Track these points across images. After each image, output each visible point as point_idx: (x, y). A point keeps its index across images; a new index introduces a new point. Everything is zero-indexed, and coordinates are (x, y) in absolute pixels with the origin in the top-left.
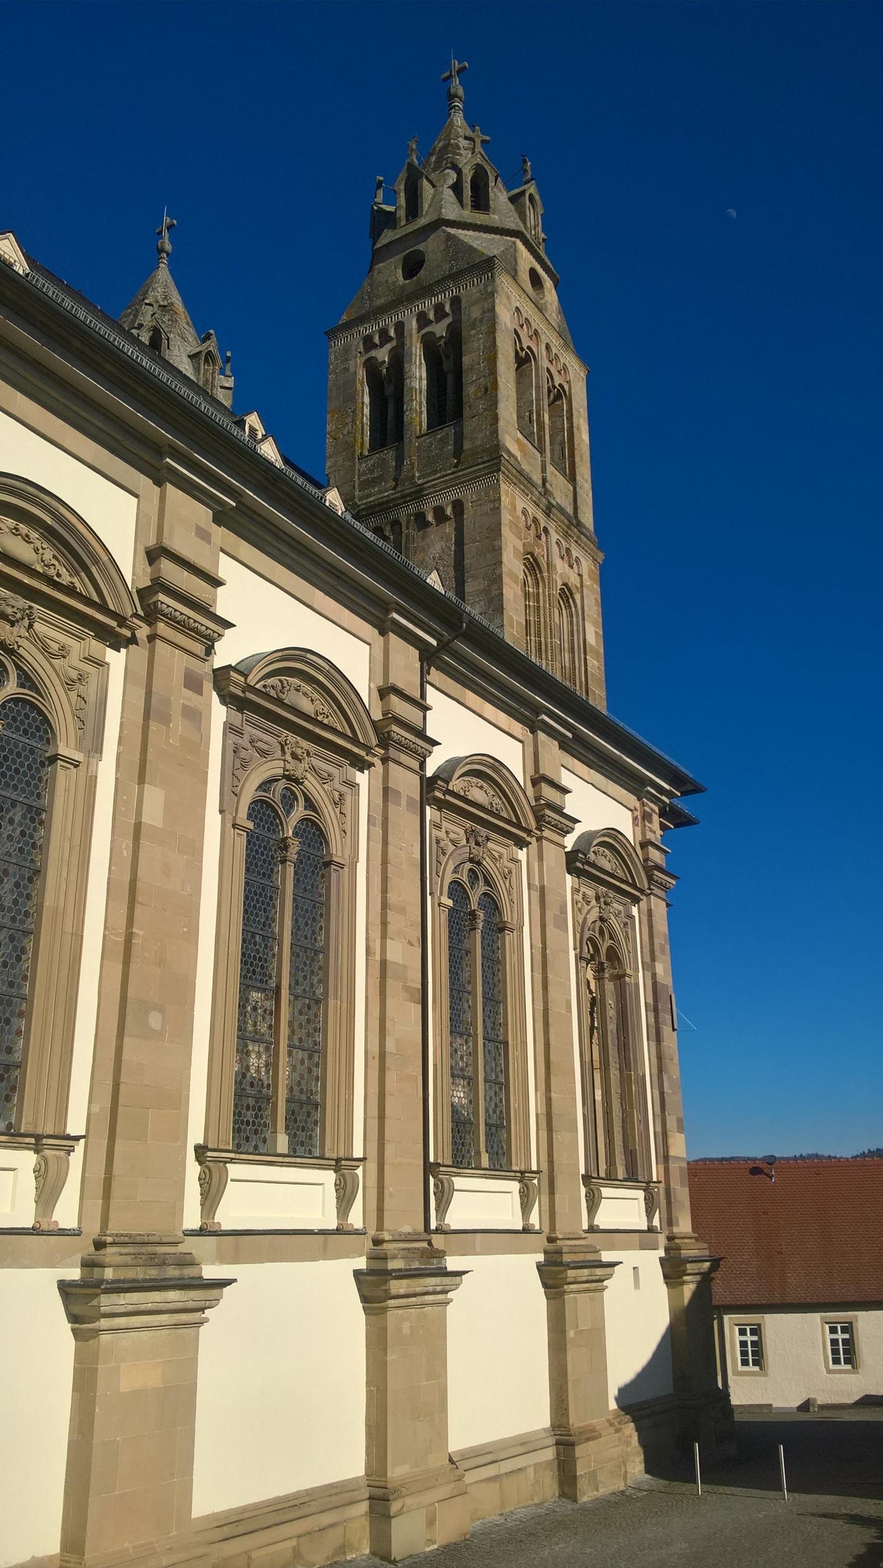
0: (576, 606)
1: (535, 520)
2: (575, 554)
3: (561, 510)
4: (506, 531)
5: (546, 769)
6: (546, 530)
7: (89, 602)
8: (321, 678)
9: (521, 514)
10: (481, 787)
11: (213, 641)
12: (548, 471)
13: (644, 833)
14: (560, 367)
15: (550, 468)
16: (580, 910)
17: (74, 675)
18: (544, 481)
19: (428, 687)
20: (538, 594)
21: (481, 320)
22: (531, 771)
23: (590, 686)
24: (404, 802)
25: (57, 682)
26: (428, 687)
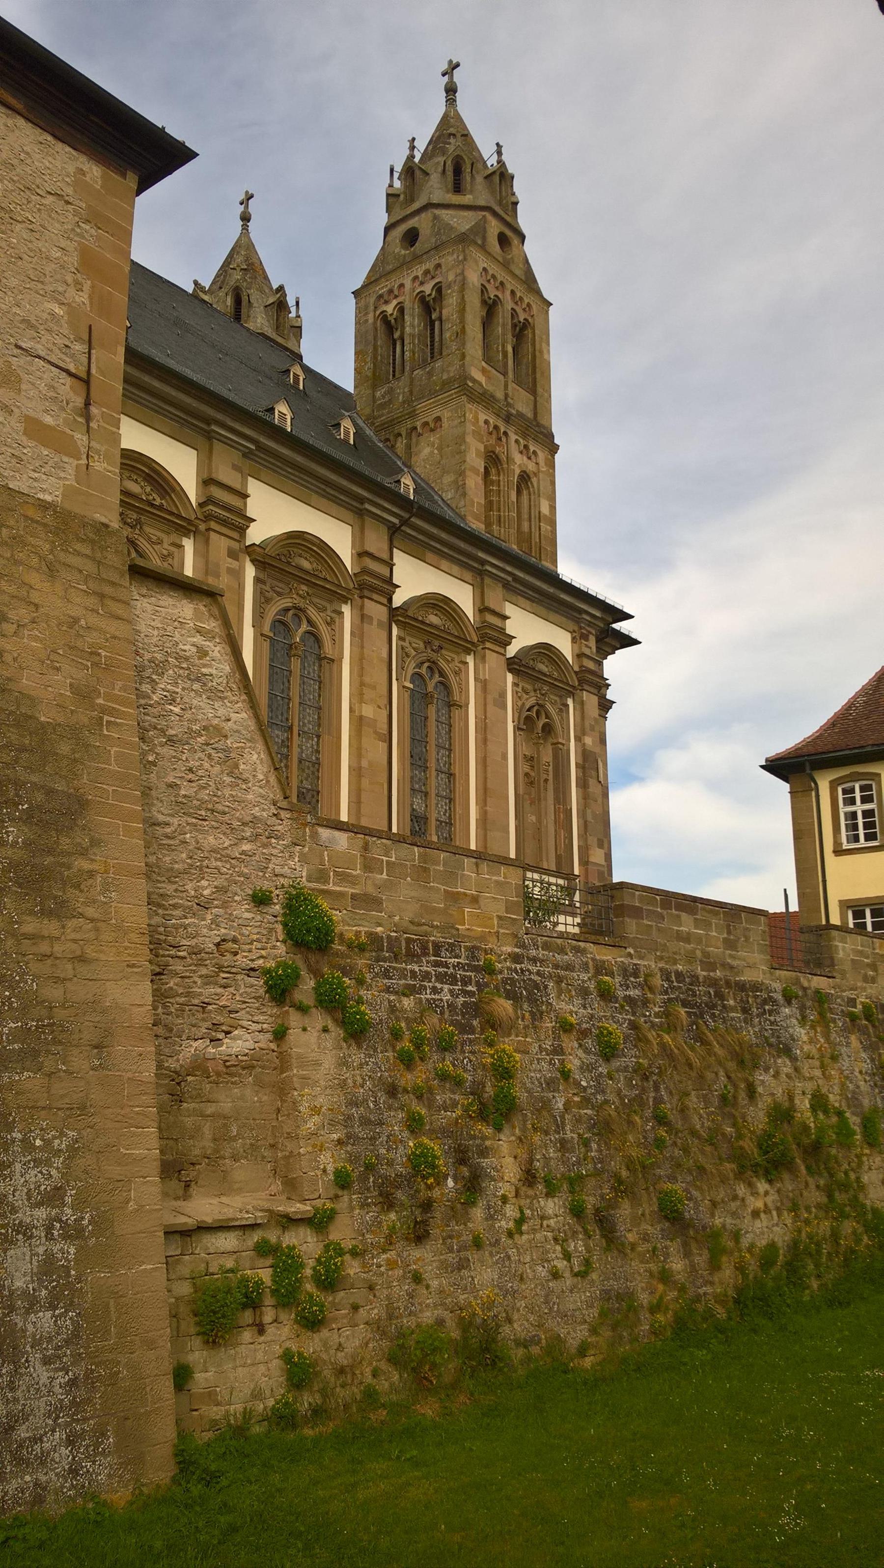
0: (533, 487)
1: (496, 427)
2: (532, 448)
3: (520, 415)
4: (469, 439)
5: (491, 603)
6: (505, 433)
7: (172, 513)
8: (315, 548)
9: (483, 424)
10: (436, 615)
11: (245, 530)
12: (509, 387)
13: (580, 648)
14: (524, 306)
15: (512, 385)
16: (520, 697)
17: (165, 552)
18: (506, 396)
19: (395, 550)
20: (499, 481)
21: (455, 281)
22: (478, 604)
23: (543, 545)
24: (375, 623)
25: (156, 557)
26: (395, 550)
